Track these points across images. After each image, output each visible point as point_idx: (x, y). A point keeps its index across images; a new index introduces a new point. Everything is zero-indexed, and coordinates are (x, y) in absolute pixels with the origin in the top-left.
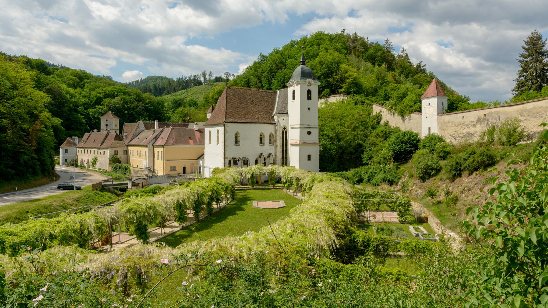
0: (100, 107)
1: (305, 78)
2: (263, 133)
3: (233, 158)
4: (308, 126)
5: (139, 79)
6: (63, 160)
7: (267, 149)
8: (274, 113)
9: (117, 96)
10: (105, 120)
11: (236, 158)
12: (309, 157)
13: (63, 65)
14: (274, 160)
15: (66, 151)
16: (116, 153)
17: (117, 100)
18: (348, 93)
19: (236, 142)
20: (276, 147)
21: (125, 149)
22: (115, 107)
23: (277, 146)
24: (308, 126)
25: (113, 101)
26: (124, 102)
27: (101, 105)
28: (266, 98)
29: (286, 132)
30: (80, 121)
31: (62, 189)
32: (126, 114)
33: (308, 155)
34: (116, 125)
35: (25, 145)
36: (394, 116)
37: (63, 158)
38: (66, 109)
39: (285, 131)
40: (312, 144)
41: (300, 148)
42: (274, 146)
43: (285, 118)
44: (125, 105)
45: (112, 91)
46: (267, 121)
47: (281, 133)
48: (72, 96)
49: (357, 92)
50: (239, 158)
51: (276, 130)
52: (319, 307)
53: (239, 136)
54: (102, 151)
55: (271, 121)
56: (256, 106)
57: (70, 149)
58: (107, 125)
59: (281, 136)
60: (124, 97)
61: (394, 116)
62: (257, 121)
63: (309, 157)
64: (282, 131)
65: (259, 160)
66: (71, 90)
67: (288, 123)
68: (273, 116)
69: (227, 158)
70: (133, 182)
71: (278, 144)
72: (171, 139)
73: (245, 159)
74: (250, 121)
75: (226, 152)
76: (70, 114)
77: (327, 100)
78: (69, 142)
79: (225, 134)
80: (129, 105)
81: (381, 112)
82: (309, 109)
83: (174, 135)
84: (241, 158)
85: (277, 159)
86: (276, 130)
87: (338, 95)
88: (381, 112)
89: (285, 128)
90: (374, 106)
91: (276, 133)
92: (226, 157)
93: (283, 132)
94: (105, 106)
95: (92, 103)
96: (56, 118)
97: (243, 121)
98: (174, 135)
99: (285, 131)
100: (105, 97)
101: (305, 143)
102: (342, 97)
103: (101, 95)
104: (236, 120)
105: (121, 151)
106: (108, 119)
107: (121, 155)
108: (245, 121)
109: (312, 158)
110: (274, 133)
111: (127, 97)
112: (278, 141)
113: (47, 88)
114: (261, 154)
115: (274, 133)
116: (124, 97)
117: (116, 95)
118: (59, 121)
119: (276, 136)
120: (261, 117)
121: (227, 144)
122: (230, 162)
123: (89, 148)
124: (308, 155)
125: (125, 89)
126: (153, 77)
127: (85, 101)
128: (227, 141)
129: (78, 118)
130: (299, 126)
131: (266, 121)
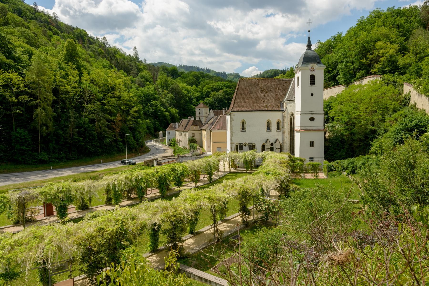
0: (208, 98)
1: (308, 63)
2: (270, 120)
3: (239, 143)
4: (311, 113)
5: (259, 74)
6: (168, 140)
7: (274, 135)
8: (285, 100)
9: (221, 89)
10: (198, 109)
11: (242, 143)
12: (312, 144)
13: (207, 68)
14: (281, 146)
15: (169, 133)
16: (193, 135)
17: (220, 92)
18: (382, 72)
19: (243, 128)
20: (284, 133)
21: (200, 132)
22: (218, 98)
23: (285, 132)
24: (311, 113)
25: (217, 93)
26: (225, 94)
27: (209, 97)
28: (279, 86)
29: (294, 118)
30: (192, 110)
31: (123, 163)
32: (226, 103)
33: (310, 142)
34: (206, 113)
35: (109, 132)
36: (421, 96)
37: (168, 138)
38: (182, 101)
39: (292, 117)
40: (315, 130)
41: (301, 135)
42: (282, 132)
43: (292, 104)
44: (226, 96)
45: (218, 86)
46: (275, 109)
47: (289, 119)
48: (189, 92)
49: (392, 72)
50: (246, 143)
51: (283, 117)
52: (279, 285)
53: (246, 124)
54: (185, 133)
55: (280, 108)
56: (267, 95)
57: (172, 132)
58: (199, 113)
59: (289, 122)
60: (226, 89)
61: (421, 96)
62: (265, 109)
63: (312, 144)
64: (290, 118)
65: (266, 145)
66: (189, 87)
67: (295, 110)
68: (283, 103)
69: (234, 143)
70: (158, 162)
71: (285, 130)
72: (218, 125)
73: (251, 145)
74: (257, 109)
75: (232, 138)
76: (186, 105)
77: (361, 82)
78: (172, 127)
79: (231, 121)
80: (229, 96)
81: (410, 92)
82: (312, 95)
83: (221, 122)
84: (247, 143)
85: (285, 145)
86: (283, 117)
87: (371, 76)
88: (410, 92)
89: (292, 115)
90: (405, 86)
91: (283, 120)
92: (233, 142)
93: (291, 119)
94: (211, 98)
95: (204, 96)
96: (174, 109)
97: (249, 109)
98: (221, 122)
99: (292, 117)
100: (213, 91)
101: (306, 130)
102: (375, 78)
103: (209, 90)
104: (243, 109)
105: (197, 133)
106: (200, 109)
107: (197, 137)
108: (252, 110)
109: (315, 144)
110: (281, 120)
111: (228, 90)
112: (285, 127)
113: (171, 87)
114: (277, 139)
115: (281, 120)
116: (226, 89)
117: (221, 88)
118: (176, 111)
119: (283, 123)
120: (269, 105)
121: (234, 131)
122: (237, 146)
123: (180, 131)
124: (310, 142)
125: (228, 84)
126: (269, 70)
127: (197, 95)
128: (234, 129)
129: (191, 108)
130: (300, 113)
131: (273, 109)
